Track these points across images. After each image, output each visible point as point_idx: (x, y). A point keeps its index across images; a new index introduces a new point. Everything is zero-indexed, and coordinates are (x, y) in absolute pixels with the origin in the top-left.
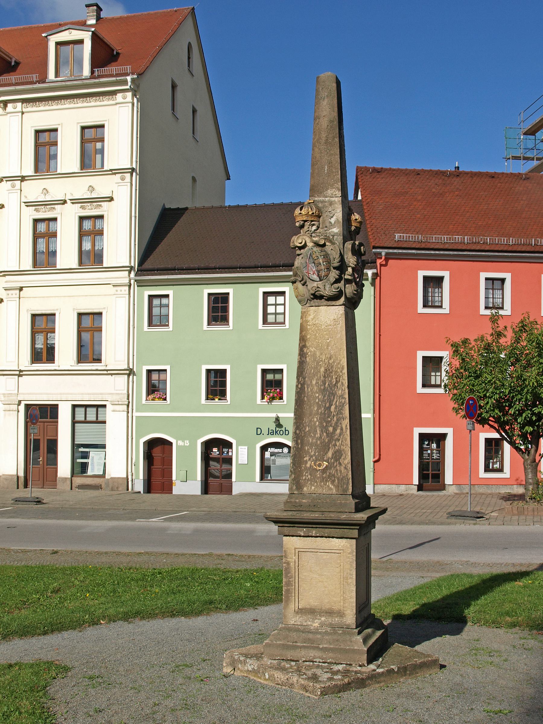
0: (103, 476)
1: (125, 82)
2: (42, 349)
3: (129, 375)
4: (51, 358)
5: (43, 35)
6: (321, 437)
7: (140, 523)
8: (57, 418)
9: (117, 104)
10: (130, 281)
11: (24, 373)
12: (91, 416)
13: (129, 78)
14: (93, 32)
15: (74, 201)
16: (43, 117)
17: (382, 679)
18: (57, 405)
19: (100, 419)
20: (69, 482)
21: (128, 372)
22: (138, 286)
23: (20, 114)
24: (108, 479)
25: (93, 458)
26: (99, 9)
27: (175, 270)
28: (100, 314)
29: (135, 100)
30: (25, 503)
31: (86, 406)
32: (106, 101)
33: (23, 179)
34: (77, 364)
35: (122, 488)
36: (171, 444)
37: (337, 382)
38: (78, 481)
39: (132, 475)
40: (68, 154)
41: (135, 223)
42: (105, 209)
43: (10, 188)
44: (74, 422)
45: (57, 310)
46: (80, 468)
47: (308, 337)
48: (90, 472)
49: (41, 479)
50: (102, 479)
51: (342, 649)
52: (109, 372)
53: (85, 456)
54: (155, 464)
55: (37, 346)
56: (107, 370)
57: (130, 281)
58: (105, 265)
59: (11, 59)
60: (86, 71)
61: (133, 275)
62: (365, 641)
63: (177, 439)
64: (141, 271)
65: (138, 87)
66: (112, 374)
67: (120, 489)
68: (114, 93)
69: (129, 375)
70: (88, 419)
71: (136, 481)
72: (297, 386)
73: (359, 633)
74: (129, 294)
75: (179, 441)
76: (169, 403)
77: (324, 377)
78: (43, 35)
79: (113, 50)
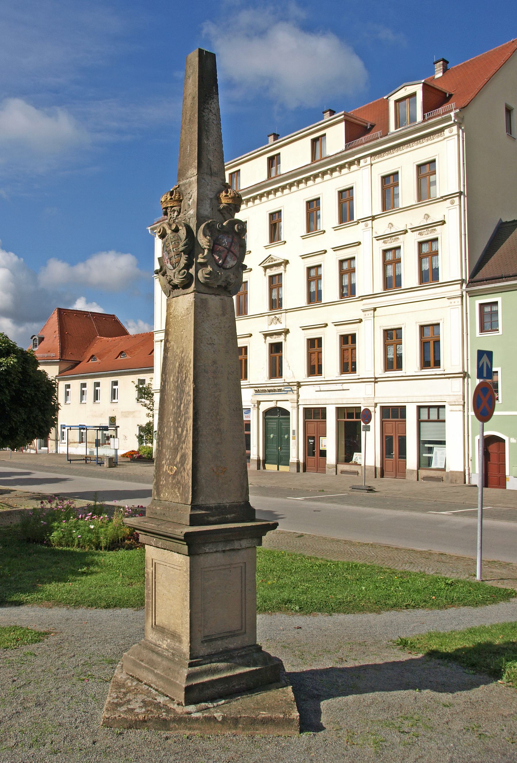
0: (444, 470)
1: (449, 119)
2: (392, 358)
3: (464, 378)
4: (399, 367)
5: (385, 98)
6: (173, 439)
7: (432, 515)
8: (405, 418)
9: (445, 139)
10: (462, 292)
11: (379, 380)
12: (434, 416)
13: (452, 114)
14: (423, 83)
15: (414, 230)
16: (385, 165)
17: (196, 725)
18: (326, 408)
19: (441, 418)
20: (415, 474)
21: (462, 375)
22: (470, 297)
23: (370, 166)
24: (448, 473)
25: (436, 453)
26: (446, 62)
27: (502, 278)
28: (438, 324)
29: (461, 131)
30: (359, 490)
31: (429, 407)
32: (436, 138)
33: (373, 218)
34: (421, 370)
35: (460, 482)
36: (503, 441)
37: (186, 377)
38: (423, 473)
39: (469, 470)
40: (407, 189)
41: (465, 241)
42: (439, 232)
43: (365, 227)
44: (419, 422)
45: (403, 324)
46: (424, 462)
47: (170, 330)
48: (433, 466)
49: (394, 471)
50: (443, 472)
51: (168, 679)
52: (446, 376)
53: (430, 450)
54: (491, 460)
55: (389, 356)
56: (444, 374)
57: (462, 292)
58: (440, 281)
59: (367, 124)
60: (419, 117)
61: (464, 286)
62: (190, 677)
63: (510, 437)
64: (472, 282)
65: (463, 119)
66: (449, 378)
67: (458, 482)
68: (442, 130)
69: (464, 378)
70: (431, 418)
71: (473, 475)
72: (161, 383)
73: (191, 665)
74: (462, 304)
75: (511, 439)
76: (500, 402)
77: (178, 373)
78: (385, 98)
79: (446, 94)
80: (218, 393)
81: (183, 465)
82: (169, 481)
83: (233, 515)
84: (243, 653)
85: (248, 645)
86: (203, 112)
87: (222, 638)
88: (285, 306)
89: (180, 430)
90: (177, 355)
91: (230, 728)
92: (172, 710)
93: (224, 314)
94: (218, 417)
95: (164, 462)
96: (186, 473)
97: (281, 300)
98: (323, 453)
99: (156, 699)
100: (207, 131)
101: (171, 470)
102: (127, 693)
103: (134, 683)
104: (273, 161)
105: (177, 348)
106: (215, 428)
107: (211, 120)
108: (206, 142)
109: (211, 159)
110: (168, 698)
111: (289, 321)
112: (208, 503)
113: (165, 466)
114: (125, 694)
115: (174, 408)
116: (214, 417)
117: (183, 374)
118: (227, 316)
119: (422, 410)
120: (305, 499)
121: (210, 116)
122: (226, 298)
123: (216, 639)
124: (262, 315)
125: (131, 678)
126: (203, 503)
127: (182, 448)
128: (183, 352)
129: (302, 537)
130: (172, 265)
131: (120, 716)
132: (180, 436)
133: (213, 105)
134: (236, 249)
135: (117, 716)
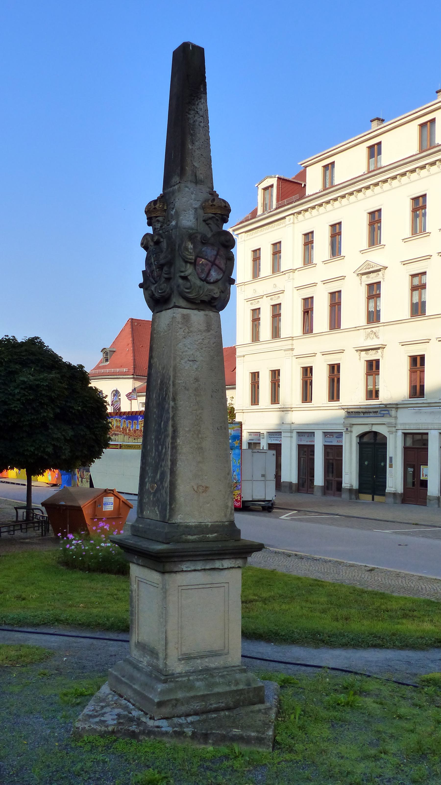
37: (166, 394)
80: (199, 411)
81: (162, 483)
82: (150, 499)
83: (216, 534)
84: (225, 673)
85: (231, 665)
86: (189, 114)
87: (202, 657)
88: (383, 319)
89: (160, 448)
90: (159, 372)
91: (200, 743)
92: (143, 723)
93: (208, 330)
94: (200, 436)
95: (147, 480)
96: (164, 492)
97: (378, 312)
98: (424, 484)
99: (131, 713)
100: (192, 135)
101: (153, 488)
102: (105, 706)
103: (116, 698)
104: (375, 151)
105: (159, 365)
106: (196, 446)
107: (197, 123)
108: (190, 147)
109: (196, 164)
110: (143, 713)
111: (384, 335)
112: (188, 521)
113: (148, 484)
114: (102, 707)
115: (155, 425)
116: (195, 436)
117: (163, 392)
118: (212, 332)
119: (239, 426)
120: (394, 532)
121: (196, 118)
122: (211, 314)
123: (195, 658)
124: (356, 329)
125: (113, 693)
126: (181, 521)
127: (161, 466)
128: (164, 368)
129: (373, 572)
130: (154, 279)
131: (90, 726)
132: (160, 454)
133: (201, 106)
134: (221, 262)
135: (86, 726)
